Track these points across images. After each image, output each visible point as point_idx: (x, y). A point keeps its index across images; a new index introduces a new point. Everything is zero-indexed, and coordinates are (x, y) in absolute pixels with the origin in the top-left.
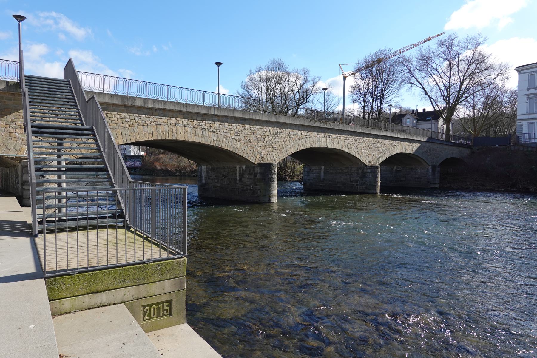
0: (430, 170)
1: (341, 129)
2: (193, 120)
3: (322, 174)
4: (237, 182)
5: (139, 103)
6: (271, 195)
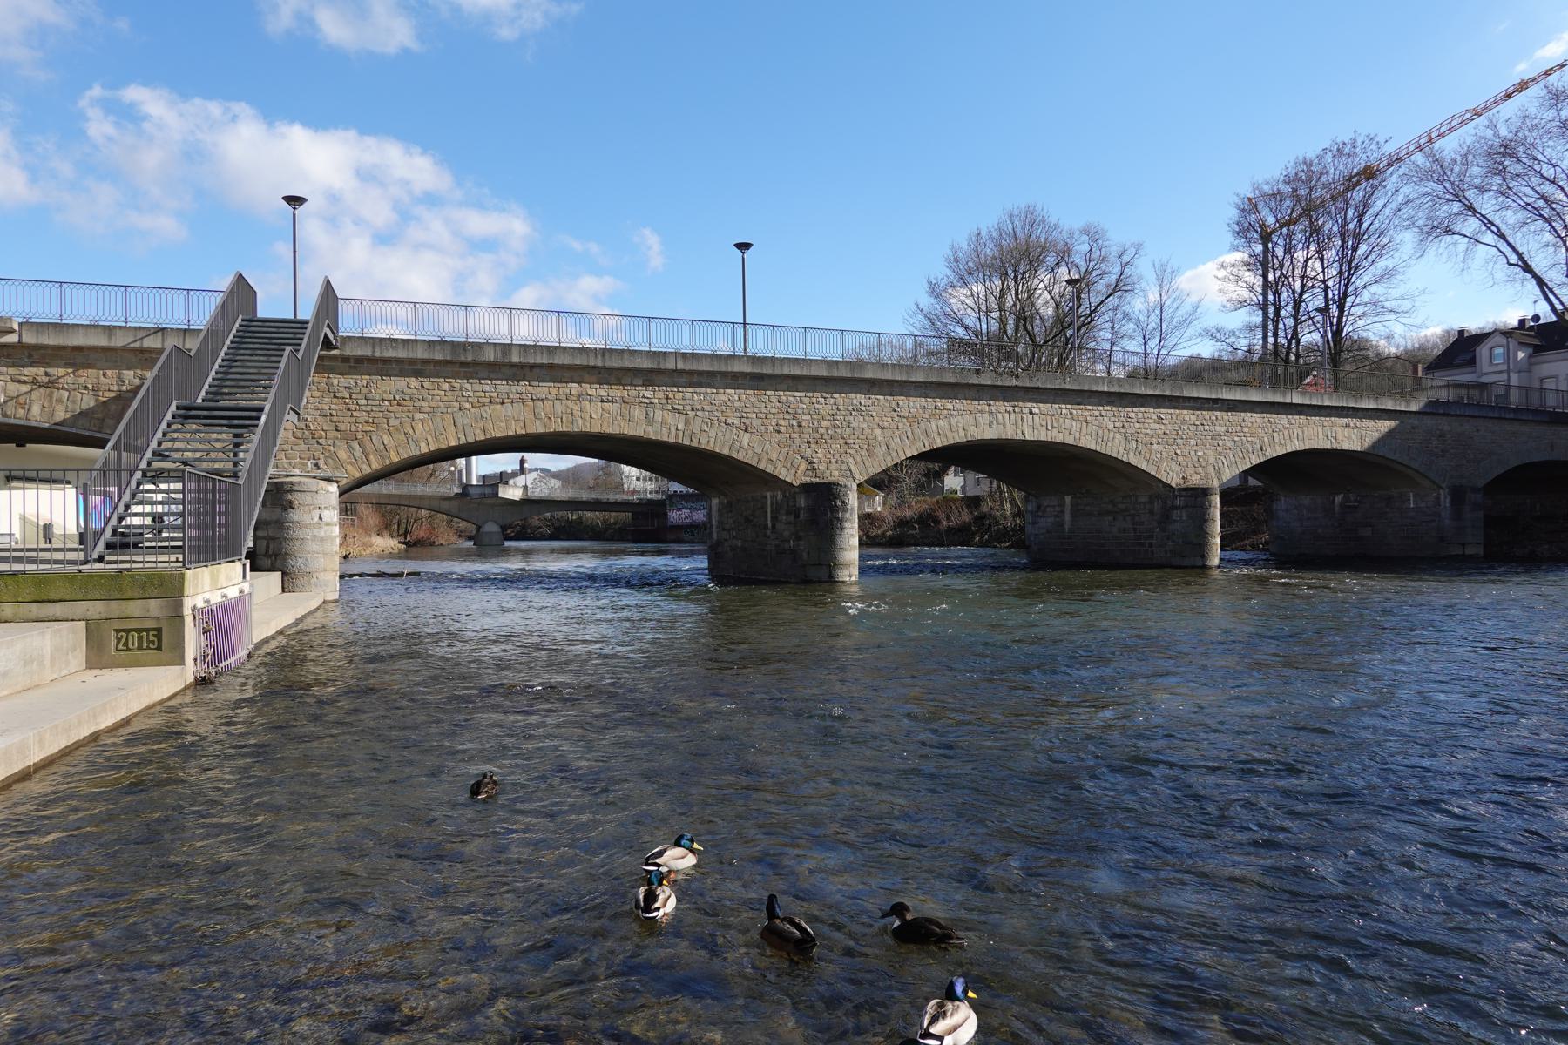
0: (1446, 502)
1: (1068, 387)
2: (623, 385)
3: (1067, 517)
4: (769, 532)
5: (490, 355)
6: (835, 564)
